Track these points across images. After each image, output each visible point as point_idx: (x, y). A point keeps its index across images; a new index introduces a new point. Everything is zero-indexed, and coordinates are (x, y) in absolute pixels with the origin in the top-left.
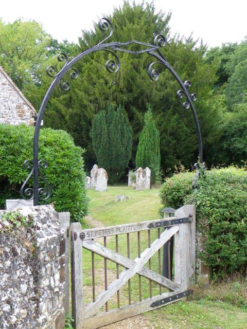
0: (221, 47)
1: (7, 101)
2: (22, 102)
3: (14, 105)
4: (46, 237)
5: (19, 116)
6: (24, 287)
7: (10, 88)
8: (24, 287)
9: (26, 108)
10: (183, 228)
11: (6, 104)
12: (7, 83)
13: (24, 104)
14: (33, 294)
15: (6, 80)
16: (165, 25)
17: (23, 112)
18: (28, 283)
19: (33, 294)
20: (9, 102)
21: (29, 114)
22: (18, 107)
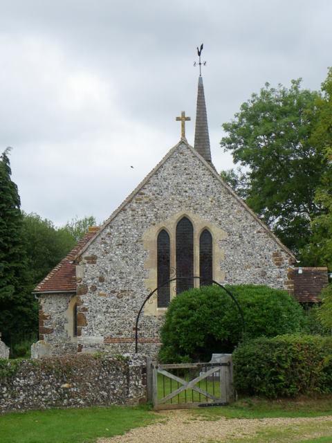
0: (43, 219)
1: (263, 250)
2: (279, 249)
3: (271, 253)
4: (133, 365)
5: (277, 264)
6: (121, 382)
7: (266, 236)
8: (121, 382)
9: (284, 255)
10: (223, 369)
11: (262, 253)
12: (263, 230)
13: (282, 251)
14: (126, 386)
15: (261, 227)
16: (235, 127)
17: (281, 260)
18: (124, 381)
19: (126, 386)
20: (265, 250)
21: (287, 261)
22: (276, 255)
